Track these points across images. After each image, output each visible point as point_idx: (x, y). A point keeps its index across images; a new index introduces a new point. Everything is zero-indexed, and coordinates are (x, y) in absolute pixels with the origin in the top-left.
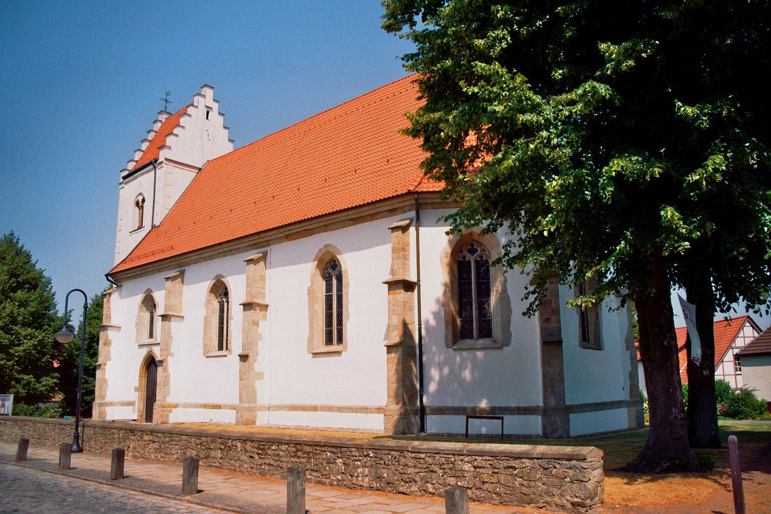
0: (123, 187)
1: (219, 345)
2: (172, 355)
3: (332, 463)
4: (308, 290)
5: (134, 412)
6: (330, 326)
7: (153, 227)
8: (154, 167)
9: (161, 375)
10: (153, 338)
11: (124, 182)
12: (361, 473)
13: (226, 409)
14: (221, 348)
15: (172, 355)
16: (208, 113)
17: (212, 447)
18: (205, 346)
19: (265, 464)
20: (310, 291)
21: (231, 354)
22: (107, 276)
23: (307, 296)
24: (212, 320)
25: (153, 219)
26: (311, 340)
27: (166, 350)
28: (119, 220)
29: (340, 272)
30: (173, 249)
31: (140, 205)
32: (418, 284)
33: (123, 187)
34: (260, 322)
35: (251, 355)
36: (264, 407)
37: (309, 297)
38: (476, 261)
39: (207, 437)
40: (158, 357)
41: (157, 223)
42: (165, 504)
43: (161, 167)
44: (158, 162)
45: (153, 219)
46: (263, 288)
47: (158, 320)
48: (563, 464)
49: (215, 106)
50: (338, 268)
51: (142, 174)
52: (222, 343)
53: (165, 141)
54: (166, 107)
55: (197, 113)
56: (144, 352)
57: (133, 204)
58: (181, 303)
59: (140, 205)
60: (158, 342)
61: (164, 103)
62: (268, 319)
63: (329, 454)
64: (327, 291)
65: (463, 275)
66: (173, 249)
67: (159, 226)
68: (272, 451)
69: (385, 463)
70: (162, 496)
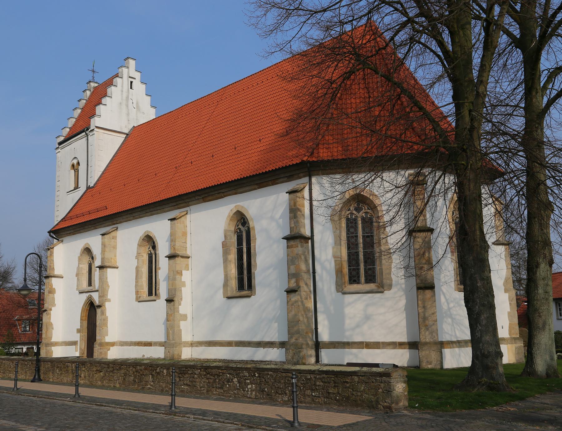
0: (59, 152)
1: (149, 291)
2: (109, 301)
3: (231, 382)
4: (223, 244)
5: (76, 351)
6: (242, 275)
7: (88, 188)
8: (86, 134)
9: (100, 318)
10: (91, 286)
11: (60, 147)
12: (250, 388)
13: (156, 346)
14: (150, 294)
15: (109, 301)
16: (131, 82)
17: (145, 374)
18: (137, 292)
19: (184, 384)
20: (224, 245)
21: (160, 299)
22: (49, 232)
23: (222, 248)
24: (143, 270)
25: (87, 180)
26: (226, 285)
27: (103, 296)
28: (56, 181)
29: (249, 228)
30: (107, 209)
31: (75, 167)
32: (312, 238)
33: (59, 152)
34: (184, 272)
35: (176, 299)
36: (142, 343)
37: (223, 250)
38: (363, 219)
39: (141, 366)
40: (97, 302)
41: (92, 184)
42: (114, 410)
43: (92, 135)
44: (90, 130)
45: (87, 180)
46: (185, 243)
47: (96, 270)
48: (377, 379)
49: (137, 75)
50: (247, 225)
51: (76, 140)
52: (152, 290)
53: (95, 110)
54: (93, 77)
55: (121, 83)
56: (85, 296)
57: (69, 166)
58: (115, 256)
59: (75, 167)
60: (97, 288)
61: (91, 73)
62: (190, 268)
63: (228, 375)
64: (238, 245)
65: (353, 230)
66: (107, 209)
67: (93, 187)
68: (189, 375)
69: (265, 380)
70: (111, 407)
